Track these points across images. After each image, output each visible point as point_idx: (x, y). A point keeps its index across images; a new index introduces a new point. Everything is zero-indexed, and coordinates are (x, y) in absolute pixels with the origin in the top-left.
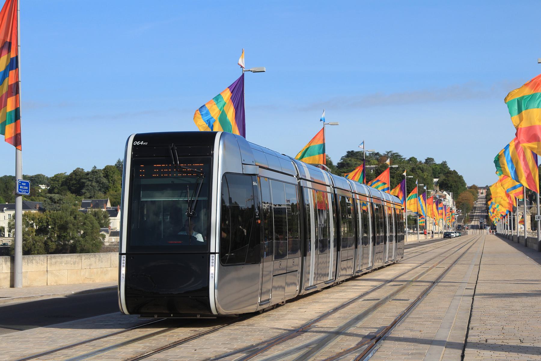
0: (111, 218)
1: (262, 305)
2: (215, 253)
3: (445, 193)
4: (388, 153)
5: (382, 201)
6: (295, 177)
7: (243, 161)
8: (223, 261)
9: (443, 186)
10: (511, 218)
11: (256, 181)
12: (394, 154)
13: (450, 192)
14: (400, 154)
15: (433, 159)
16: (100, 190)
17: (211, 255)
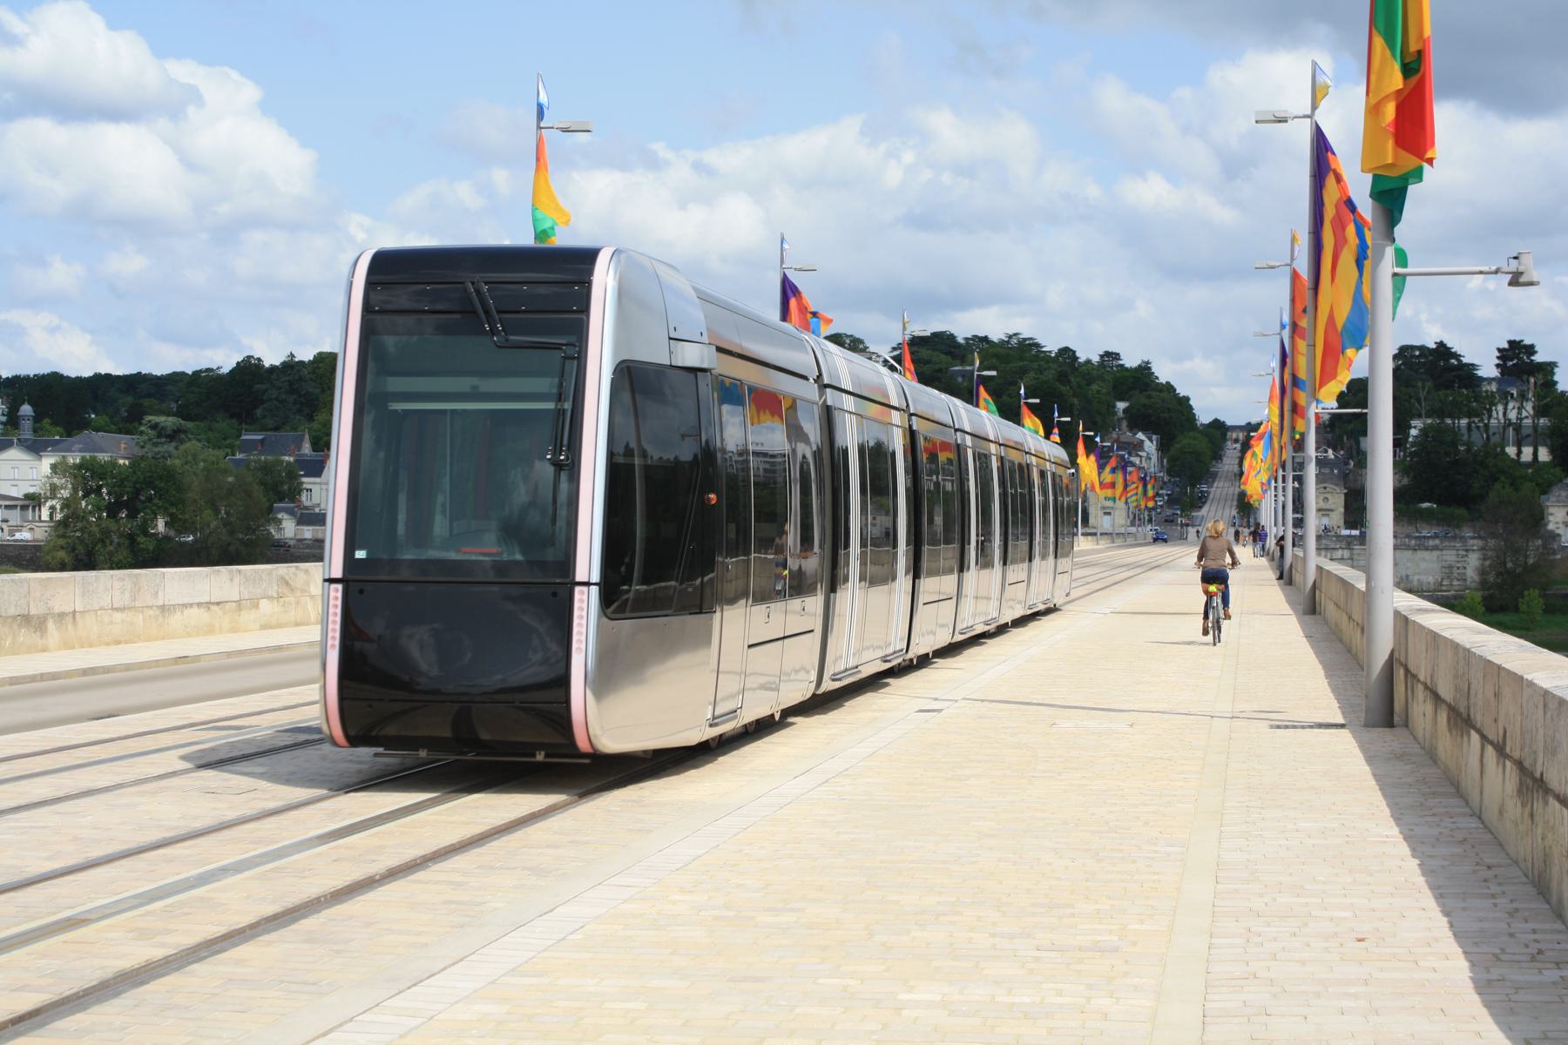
0: (304, 480)
2: (587, 584)
3: (1140, 436)
4: (1010, 337)
5: (1027, 453)
6: (812, 380)
7: (672, 330)
9: (1138, 420)
12: (1025, 340)
14: (1040, 340)
15: (1118, 354)
16: (299, 411)
17: (577, 589)
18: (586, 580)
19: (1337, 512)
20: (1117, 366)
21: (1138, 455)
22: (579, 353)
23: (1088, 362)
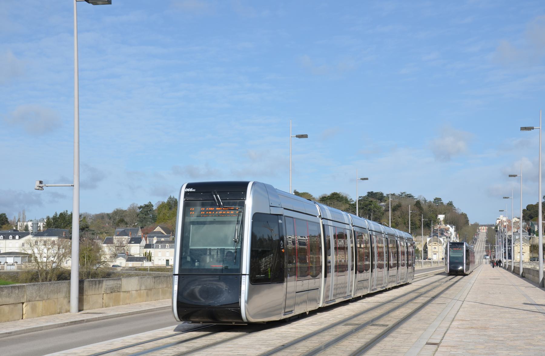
1: (285, 315)
2: (245, 275)
3: (448, 226)
4: (402, 193)
6: (318, 217)
8: (254, 281)
10: (506, 249)
11: (281, 219)
12: (408, 195)
13: (453, 225)
15: (440, 199)
17: (243, 276)
18: (245, 274)
19: (527, 253)
20: (440, 203)
21: (447, 233)
22: (243, 210)
23: (430, 202)
